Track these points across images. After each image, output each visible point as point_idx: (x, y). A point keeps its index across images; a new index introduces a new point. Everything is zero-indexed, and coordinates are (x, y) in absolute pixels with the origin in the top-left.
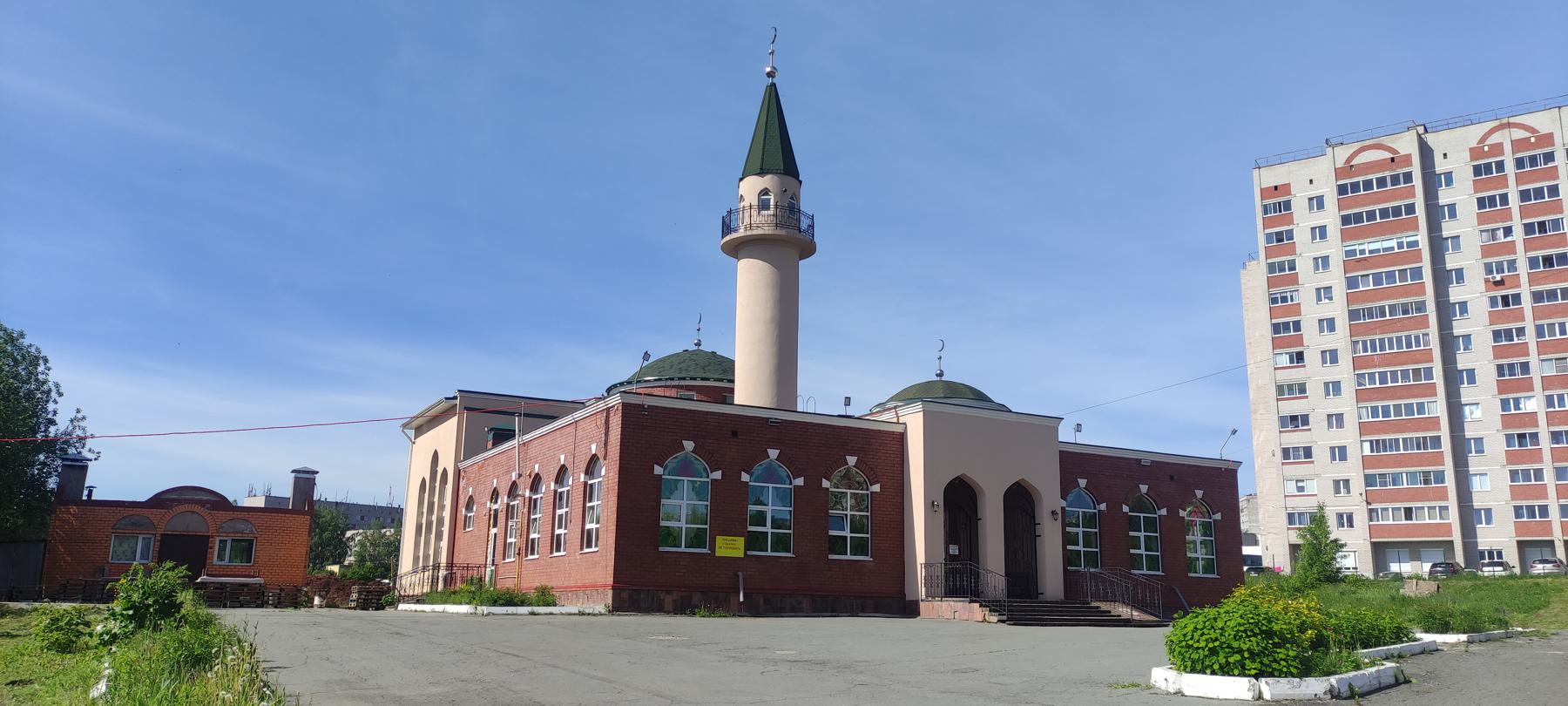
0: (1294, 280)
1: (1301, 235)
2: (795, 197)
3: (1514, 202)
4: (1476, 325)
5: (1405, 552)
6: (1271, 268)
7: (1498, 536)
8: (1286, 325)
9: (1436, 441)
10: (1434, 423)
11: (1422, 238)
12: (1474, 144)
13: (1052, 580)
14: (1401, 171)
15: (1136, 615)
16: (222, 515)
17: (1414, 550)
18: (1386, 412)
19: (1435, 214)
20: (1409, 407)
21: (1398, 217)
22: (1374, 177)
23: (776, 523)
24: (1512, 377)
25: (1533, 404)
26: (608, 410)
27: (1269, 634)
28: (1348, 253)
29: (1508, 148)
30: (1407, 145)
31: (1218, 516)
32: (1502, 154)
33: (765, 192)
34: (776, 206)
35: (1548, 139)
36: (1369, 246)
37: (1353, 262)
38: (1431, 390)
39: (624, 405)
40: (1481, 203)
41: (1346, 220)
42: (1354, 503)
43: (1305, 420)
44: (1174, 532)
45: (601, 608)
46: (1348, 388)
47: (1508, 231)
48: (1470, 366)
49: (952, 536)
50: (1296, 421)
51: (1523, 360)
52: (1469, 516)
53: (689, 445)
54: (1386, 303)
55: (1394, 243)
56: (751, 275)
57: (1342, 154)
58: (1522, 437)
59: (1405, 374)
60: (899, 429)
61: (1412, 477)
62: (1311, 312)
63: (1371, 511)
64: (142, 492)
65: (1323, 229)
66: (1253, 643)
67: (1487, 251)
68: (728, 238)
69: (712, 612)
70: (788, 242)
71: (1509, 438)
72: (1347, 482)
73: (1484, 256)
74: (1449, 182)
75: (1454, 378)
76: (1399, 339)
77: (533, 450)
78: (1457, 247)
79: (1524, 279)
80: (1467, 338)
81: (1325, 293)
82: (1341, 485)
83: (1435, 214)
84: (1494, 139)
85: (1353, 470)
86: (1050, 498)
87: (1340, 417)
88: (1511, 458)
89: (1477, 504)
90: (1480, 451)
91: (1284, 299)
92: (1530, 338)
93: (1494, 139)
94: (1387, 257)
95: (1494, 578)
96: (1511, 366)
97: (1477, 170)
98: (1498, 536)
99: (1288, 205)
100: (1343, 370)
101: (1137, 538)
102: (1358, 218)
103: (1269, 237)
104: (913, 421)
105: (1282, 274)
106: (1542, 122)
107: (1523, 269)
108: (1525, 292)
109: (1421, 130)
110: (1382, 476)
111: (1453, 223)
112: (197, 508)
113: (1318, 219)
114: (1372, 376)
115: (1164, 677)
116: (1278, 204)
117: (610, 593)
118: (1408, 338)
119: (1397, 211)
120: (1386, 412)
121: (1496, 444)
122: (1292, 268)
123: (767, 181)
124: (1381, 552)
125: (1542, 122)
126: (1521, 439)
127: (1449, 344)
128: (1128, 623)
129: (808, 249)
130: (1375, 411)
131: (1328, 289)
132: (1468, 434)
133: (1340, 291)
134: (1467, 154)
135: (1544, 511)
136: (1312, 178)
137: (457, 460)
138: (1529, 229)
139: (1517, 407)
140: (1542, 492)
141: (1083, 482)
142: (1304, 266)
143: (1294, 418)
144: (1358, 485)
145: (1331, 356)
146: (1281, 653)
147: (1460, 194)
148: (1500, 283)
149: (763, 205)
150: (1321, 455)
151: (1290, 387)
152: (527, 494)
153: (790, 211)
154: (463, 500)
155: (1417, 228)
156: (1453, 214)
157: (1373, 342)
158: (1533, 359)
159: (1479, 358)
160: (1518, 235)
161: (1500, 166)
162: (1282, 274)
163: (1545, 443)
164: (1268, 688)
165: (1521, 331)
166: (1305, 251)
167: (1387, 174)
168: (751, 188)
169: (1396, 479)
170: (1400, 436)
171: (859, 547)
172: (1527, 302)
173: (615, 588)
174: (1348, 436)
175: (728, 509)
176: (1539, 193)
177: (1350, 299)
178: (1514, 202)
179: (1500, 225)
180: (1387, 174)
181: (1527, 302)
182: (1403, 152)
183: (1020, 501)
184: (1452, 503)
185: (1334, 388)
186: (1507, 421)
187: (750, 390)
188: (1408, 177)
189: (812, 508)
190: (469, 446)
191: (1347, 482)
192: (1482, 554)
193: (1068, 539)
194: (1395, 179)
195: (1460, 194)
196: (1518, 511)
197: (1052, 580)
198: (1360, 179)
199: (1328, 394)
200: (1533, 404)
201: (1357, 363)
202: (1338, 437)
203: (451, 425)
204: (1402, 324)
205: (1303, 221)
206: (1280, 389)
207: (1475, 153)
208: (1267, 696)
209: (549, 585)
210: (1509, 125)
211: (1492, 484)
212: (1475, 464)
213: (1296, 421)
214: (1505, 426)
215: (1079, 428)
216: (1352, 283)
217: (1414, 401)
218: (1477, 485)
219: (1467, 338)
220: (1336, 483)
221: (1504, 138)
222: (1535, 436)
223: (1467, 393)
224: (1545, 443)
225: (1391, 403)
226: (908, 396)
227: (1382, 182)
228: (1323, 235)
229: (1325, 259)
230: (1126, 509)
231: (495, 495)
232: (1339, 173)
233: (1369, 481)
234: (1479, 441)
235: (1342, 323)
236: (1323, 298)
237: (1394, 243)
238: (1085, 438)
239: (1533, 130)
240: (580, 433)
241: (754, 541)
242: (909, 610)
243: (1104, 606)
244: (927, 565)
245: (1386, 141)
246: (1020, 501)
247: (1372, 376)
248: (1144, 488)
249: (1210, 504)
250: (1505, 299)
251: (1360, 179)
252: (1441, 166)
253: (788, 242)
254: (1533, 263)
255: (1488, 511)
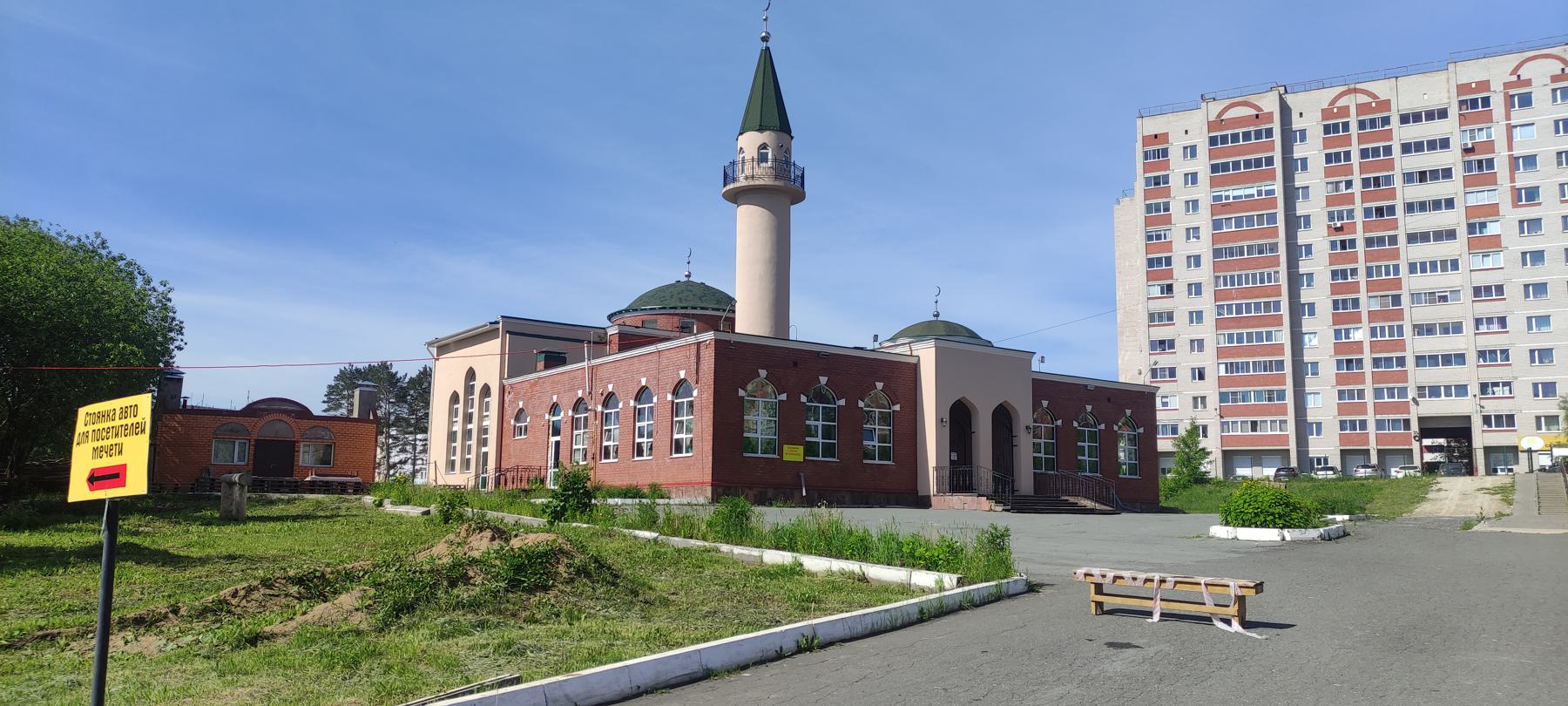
0: (1167, 220)
1: (1176, 181)
2: (788, 151)
3: (1355, 158)
4: (1317, 265)
5: (1248, 459)
6: (1149, 208)
7: (1326, 446)
8: (1159, 260)
9: (1280, 364)
10: (1279, 349)
11: (1278, 187)
12: (1325, 106)
13: (1025, 481)
14: (1264, 127)
15: (1098, 506)
16: (305, 423)
17: (1256, 458)
18: (1240, 339)
19: (1290, 166)
20: (1259, 335)
21: (1257, 168)
22: (1240, 131)
23: (882, 439)
24: (1345, 311)
25: (1360, 335)
26: (699, 344)
27: (1287, 505)
28: (1216, 198)
29: (1353, 110)
30: (1270, 104)
31: (1141, 430)
32: (1348, 115)
33: (764, 146)
34: (775, 160)
35: (1385, 105)
36: (1233, 192)
37: (1219, 206)
38: (1278, 321)
39: (717, 341)
40: (1329, 158)
41: (1214, 168)
42: (1209, 417)
43: (1171, 344)
44: (1107, 445)
45: (701, 500)
46: (1210, 317)
47: (1349, 184)
48: (1311, 300)
49: (953, 446)
50: (1164, 345)
51: (1354, 296)
52: (1304, 429)
53: (763, 373)
54: (1245, 244)
55: (1254, 191)
56: (750, 221)
57: (1214, 109)
58: (1349, 361)
59: (1257, 305)
60: (914, 361)
61: (1258, 394)
62: (1181, 249)
63: (1223, 424)
64: (237, 401)
65: (1194, 175)
66: (1279, 510)
67: (1330, 201)
68: (731, 186)
69: (785, 504)
70: (782, 192)
71: (1339, 362)
72: (1203, 398)
73: (1328, 205)
74: (1303, 138)
75: (1297, 310)
76: (1254, 275)
77: (602, 373)
78: (1306, 196)
79: (1359, 227)
80: (1310, 276)
81: (1192, 233)
82: (1200, 401)
83: (1290, 166)
84: (1342, 102)
85: (1209, 388)
86: (1024, 415)
87: (1201, 342)
88: (1340, 379)
89: (1310, 419)
90: (1315, 373)
91: (1159, 237)
92: (1362, 278)
93: (1342, 102)
94: (1249, 203)
95: (1329, 480)
96: (1344, 301)
97: (1327, 129)
98: (1326, 446)
99: (1165, 152)
100: (1206, 303)
101: (1086, 447)
102: (1225, 167)
103: (1148, 181)
104: (926, 355)
105: (1157, 214)
106: (1382, 89)
107: (1359, 217)
108: (1360, 236)
109: (1282, 90)
110: (1234, 393)
111: (1304, 175)
112: (284, 417)
113: (1191, 166)
114: (1229, 307)
115: (1220, 531)
116: (1157, 150)
117: (709, 490)
118: (1262, 274)
119: (1258, 163)
120: (1240, 339)
121: (1328, 369)
122: (1167, 209)
123: (765, 137)
124: (1229, 457)
125: (1382, 89)
126: (1349, 364)
127: (1295, 280)
128: (1092, 512)
129: (799, 197)
130: (1230, 337)
131: (1196, 229)
132: (1306, 359)
133: (1206, 232)
134: (1320, 114)
135: (1363, 424)
136: (1188, 129)
137: (501, 378)
138: (1366, 183)
139: (1347, 337)
140: (1362, 409)
141: (880, 385)
142: (1177, 208)
143: (1162, 342)
144: (1213, 401)
145: (1196, 289)
146: (1294, 515)
147: (1311, 150)
148: (1339, 230)
149: (763, 158)
150: (1184, 374)
151: (1160, 315)
152: (600, 408)
153: (784, 165)
154: (510, 413)
155: (1274, 178)
156: (1304, 168)
157: (1232, 277)
158: (1363, 296)
159: (1319, 294)
160: (1357, 187)
161: (1346, 126)
162: (1157, 214)
163: (1368, 367)
164: (1288, 534)
165: (1354, 272)
166: (1179, 194)
167: (1252, 129)
168: (750, 142)
169: (1245, 397)
170: (1251, 360)
171: (884, 454)
172: (1360, 247)
173: (715, 484)
174: (1207, 359)
175: (790, 426)
176: (1376, 151)
177: (1215, 239)
178: (1355, 158)
179: (1344, 178)
180: (1252, 129)
181: (1360, 247)
182: (1266, 110)
183: (1003, 417)
184: (1291, 418)
185: (1196, 317)
186: (1339, 348)
187: (750, 321)
188: (1269, 133)
189: (850, 425)
190: (515, 365)
191: (1203, 398)
192: (1311, 460)
193: (1037, 448)
194: (1258, 134)
195: (1311, 150)
196: (1343, 424)
197: (1025, 481)
198: (1229, 132)
199: (1191, 321)
200: (1360, 335)
201: (1218, 295)
202: (1198, 360)
203: (494, 345)
204: (1256, 260)
205: (1178, 167)
206: (1151, 317)
207: (1326, 114)
208: (1288, 538)
209: (658, 482)
210: (1355, 91)
211: (1323, 403)
212: (1310, 384)
213: (1164, 345)
214: (1337, 352)
215: (1042, 360)
216: (1217, 225)
217: (1264, 330)
218: (1311, 402)
219: (1310, 276)
220: (1195, 399)
221: (1350, 101)
222: (1360, 362)
223: (1307, 324)
224: (1368, 367)
225: (1244, 331)
226: (919, 332)
227: (1247, 136)
228: (1194, 181)
229: (1195, 202)
230: (1075, 424)
231: (554, 409)
232: (1211, 126)
233: (1223, 397)
234: (1315, 364)
235: (1207, 260)
236: (1192, 238)
237: (1254, 191)
238: (1045, 368)
239: (1374, 96)
240: (664, 362)
241: (810, 449)
242: (924, 503)
243: (1072, 499)
244: (937, 468)
245: (1253, 99)
246: (1003, 417)
247: (1229, 307)
248: (823, 380)
249: (1133, 423)
250: (1343, 243)
251: (1229, 132)
252: (1297, 124)
253: (782, 192)
254: (1367, 212)
255: (1319, 425)
